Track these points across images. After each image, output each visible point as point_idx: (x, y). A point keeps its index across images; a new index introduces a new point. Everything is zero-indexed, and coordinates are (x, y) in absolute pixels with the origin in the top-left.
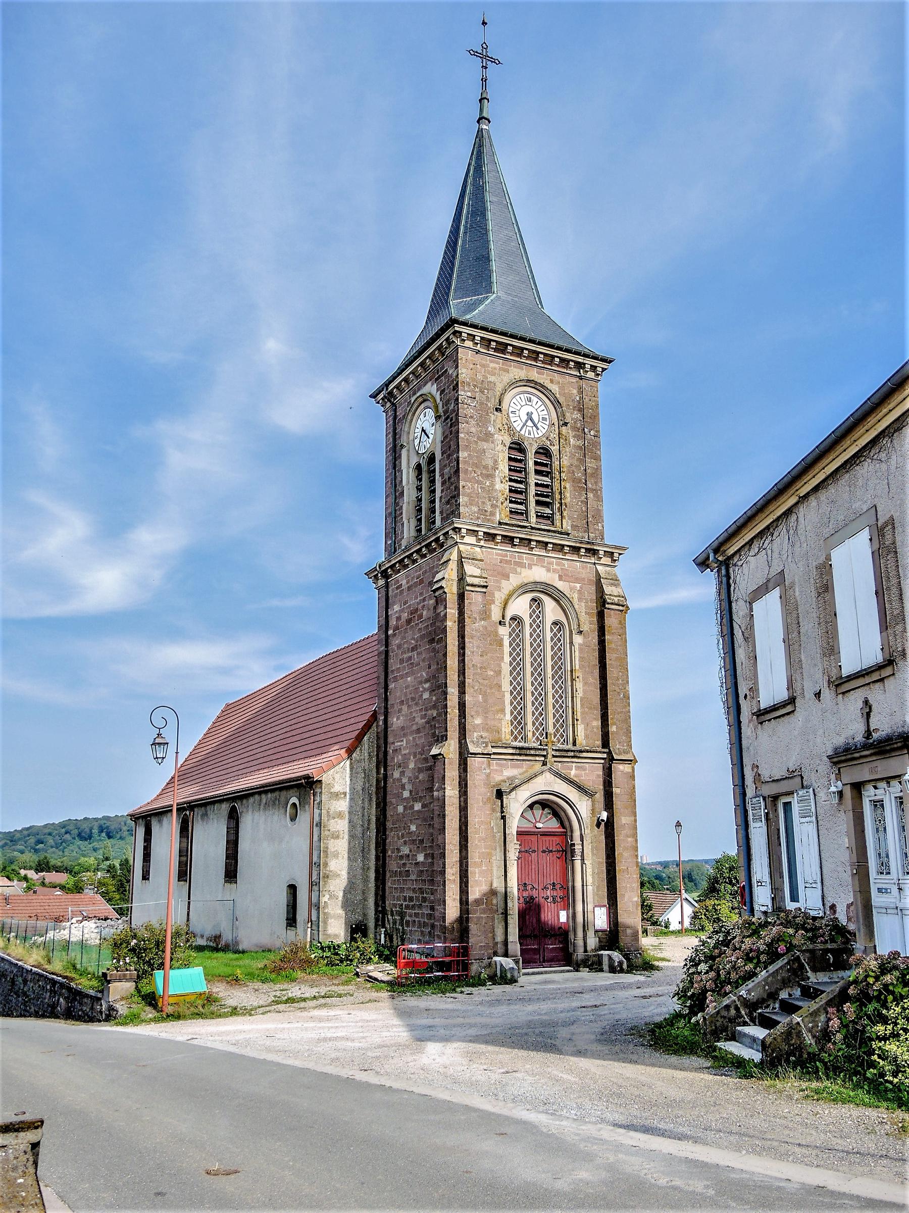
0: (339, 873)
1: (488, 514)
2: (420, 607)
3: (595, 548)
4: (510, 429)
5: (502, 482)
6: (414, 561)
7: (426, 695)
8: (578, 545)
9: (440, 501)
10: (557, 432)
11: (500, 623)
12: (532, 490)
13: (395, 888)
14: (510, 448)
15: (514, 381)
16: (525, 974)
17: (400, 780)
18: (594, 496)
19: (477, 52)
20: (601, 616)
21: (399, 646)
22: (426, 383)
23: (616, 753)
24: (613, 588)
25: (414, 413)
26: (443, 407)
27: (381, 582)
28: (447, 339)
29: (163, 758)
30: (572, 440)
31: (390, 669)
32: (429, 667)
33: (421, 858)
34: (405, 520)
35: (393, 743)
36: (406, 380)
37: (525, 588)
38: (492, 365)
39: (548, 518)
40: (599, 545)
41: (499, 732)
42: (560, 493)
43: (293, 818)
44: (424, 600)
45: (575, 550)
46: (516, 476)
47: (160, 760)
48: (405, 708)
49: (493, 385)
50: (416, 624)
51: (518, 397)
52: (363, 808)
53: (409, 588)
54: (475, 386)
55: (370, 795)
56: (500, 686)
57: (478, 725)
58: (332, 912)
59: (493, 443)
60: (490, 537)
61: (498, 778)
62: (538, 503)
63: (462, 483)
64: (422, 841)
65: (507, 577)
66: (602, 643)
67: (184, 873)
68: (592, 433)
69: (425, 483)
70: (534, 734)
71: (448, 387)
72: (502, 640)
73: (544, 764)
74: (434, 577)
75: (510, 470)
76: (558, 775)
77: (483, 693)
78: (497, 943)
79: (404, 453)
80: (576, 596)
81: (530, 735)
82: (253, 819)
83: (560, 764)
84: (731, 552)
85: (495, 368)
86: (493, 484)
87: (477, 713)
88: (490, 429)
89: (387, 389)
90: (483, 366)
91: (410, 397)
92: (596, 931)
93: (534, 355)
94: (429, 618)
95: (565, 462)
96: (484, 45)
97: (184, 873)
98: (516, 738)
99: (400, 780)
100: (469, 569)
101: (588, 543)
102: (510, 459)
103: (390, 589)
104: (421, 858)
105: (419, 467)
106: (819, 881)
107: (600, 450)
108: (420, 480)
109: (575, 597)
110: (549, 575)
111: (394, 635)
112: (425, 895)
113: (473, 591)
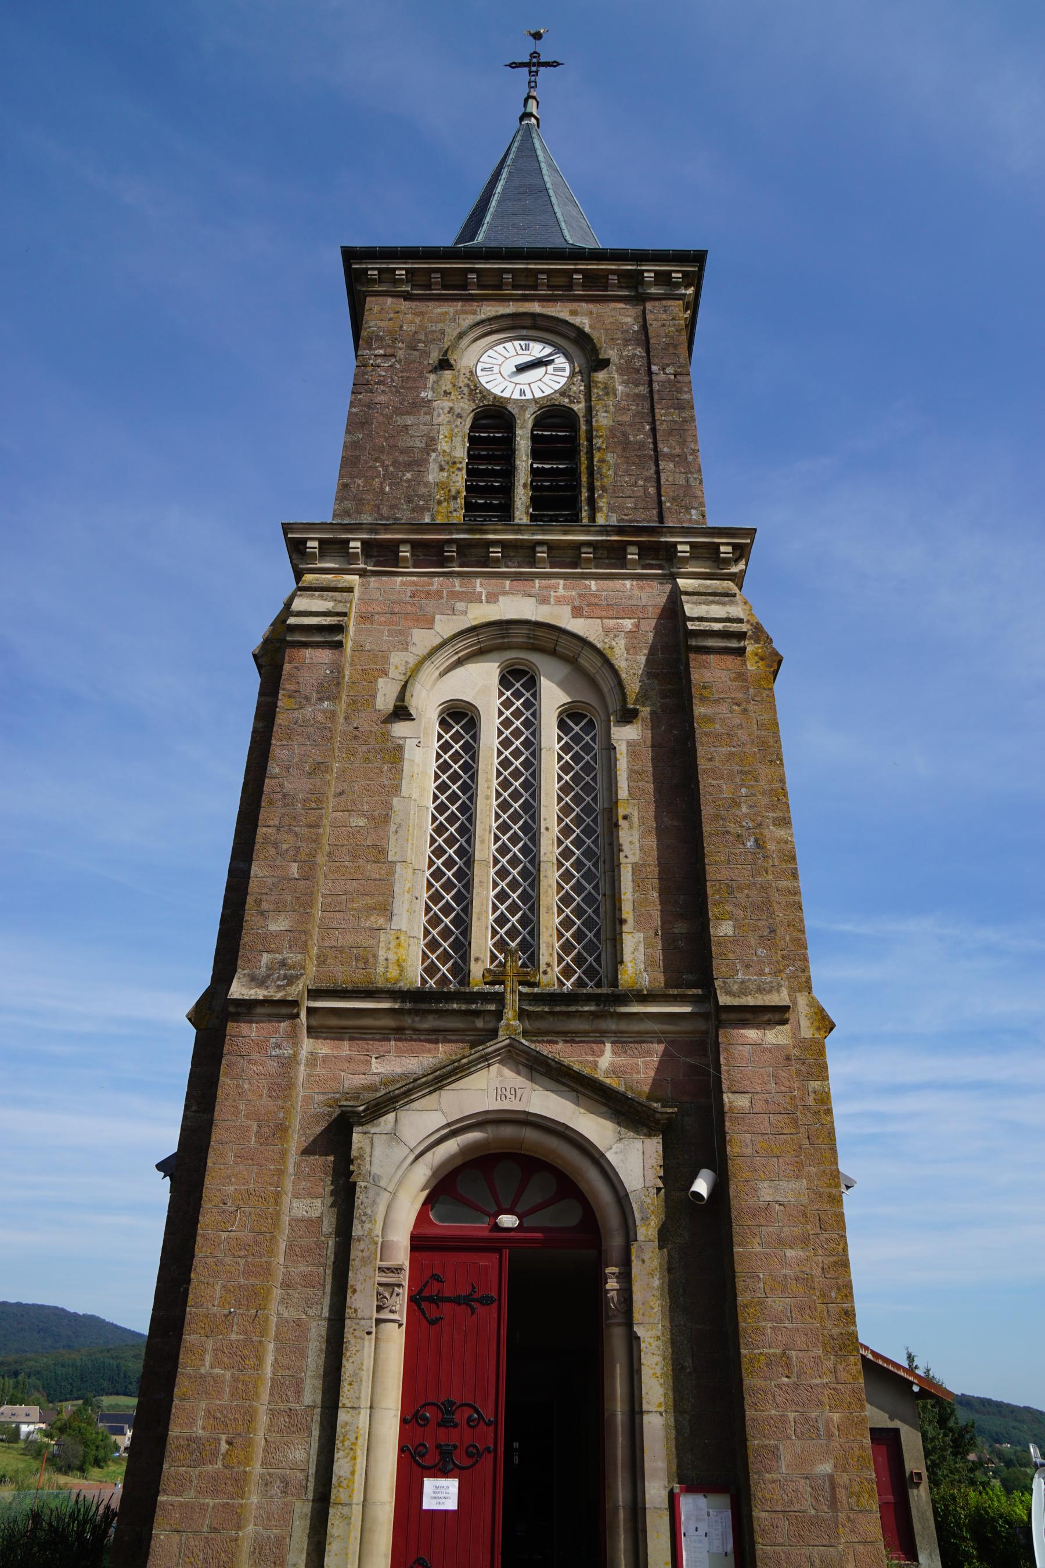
4: (475, 390)
40: (672, 531)
65: (428, 623)
77: (303, 856)
87: (280, 908)
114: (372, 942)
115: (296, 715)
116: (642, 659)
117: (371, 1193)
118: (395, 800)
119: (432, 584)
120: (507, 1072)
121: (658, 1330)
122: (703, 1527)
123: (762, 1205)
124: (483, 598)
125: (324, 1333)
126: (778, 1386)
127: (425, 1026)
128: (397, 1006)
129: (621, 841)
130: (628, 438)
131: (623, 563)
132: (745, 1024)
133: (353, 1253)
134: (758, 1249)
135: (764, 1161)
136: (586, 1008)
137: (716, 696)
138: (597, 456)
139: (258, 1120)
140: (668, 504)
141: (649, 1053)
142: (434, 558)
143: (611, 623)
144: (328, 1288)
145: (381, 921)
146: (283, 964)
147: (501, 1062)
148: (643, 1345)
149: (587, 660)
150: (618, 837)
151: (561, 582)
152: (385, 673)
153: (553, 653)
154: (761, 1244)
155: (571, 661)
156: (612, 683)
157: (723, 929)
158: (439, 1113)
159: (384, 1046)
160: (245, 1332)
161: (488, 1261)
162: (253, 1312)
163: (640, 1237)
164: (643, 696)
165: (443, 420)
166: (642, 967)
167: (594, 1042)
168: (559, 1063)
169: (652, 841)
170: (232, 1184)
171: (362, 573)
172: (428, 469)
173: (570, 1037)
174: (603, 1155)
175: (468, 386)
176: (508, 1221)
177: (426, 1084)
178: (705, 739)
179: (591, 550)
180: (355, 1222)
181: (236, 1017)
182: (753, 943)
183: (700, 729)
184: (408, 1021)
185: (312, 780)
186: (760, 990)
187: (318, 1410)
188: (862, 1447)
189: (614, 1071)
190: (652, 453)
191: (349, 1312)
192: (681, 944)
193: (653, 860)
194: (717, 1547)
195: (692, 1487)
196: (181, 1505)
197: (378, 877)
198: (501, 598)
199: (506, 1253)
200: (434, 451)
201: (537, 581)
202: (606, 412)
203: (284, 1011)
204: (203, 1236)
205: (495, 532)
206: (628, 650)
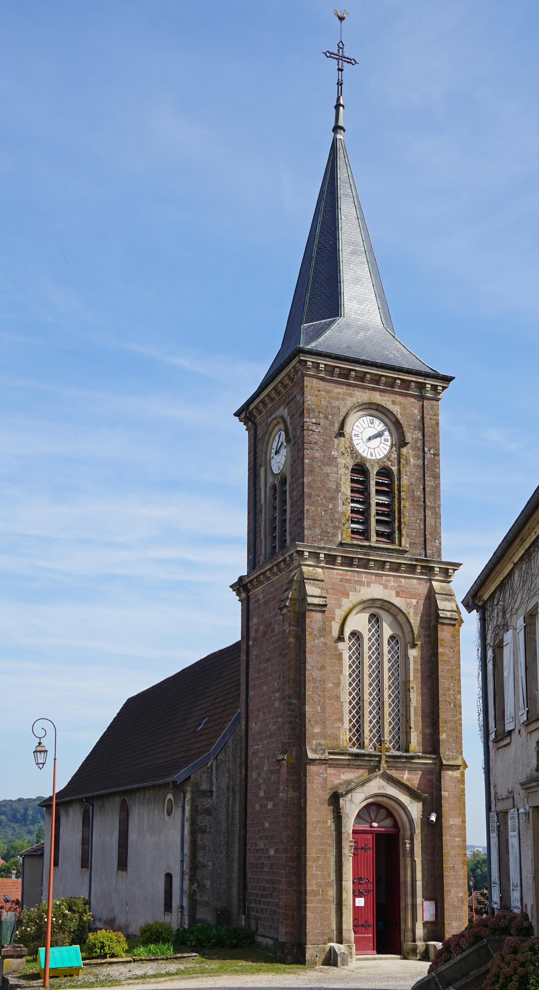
0: (206, 863)
1: (330, 535)
2: (273, 621)
4: (353, 452)
5: (344, 504)
7: (277, 704)
9: (290, 522)
13: (254, 879)
14: (352, 469)
15: (357, 404)
16: (358, 960)
17: (257, 780)
18: (432, 513)
21: (257, 656)
22: (280, 406)
23: (445, 759)
24: (447, 603)
26: (292, 432)
29: (43, 764)
30: (412, 460)
31: (250, 678)
35: (252, 746)
36: (262, 401)
40: (434, 562)
41: (336, 738)
43: (169, 813)
45: (412, 568)
47: (41, 766)
48: (261, 714)
49: (336, 410)
50: (270, 637)
51: (361, 420)
52: (228, 805)
53: (265, 603)
54: (319, 412)
55: (234, 793)
56: (339, 697)
57: (317, 733)
58: (200, 899)
60: (331, 559)
62: (378, 522)
63: (306, 507)
65: (347, 595)
67: (86, 862)
68: (432, 452)
70: (371, 741)
72: (341, 654)
75: (352, 491)
77: (321, 704)
80: (412, 611)
81: (367, 742)
82: (139, 812)
84: (486, 597)
85: (339, 393)
86: (335, 506)
87: (317, 722)
88: (333, 453)
90: (328, 392)
91: (267, 418)
93: (377, 380)
94: (279, 633)
95: (405, 481)
97: (86, 862)
98: (354, 745)
99: (257, 780)
102: (353, 481)
103: (251, 602)
104: (272, 852)
105: (274, 487)
106: (519, 885)
107: (439, 468)
110: (387, 591)
111: (253, 645)
112: (275, 886)
114: (338, 732)
115: (313, 643)
116: (419, 619)
117: (347, 819)
118: (341, 676)
119: (347, 575)
120: (381, 781)
121: (420, 859)
122: (428, 909)
123: (450, 825)
124: (365, 584)
125: (334, 860)
126: (452, 875)
127: (357, 764)
128: (350, 758)
129: (411, 697)
130: (414, 494)
131: (414, 572)
132: (448, 770)
133: (343, 837)
134: (448, 838)
135: (451, 812)
136: (403, 760)
137: (445, 645)
138: (402, 503)
139: (319, 798)
140: (428, 536)
141: (417, 774)
142: (347, 562)
143: (408, 600)
144: (335, 847)
146: (320, 744)
147: (379, 777)
148: (417, 863)
149: (400, 617)
150: (410, 695)
151: (392, 578)
152: (334, 619)
153: (388, 611)
154: (449, 836)
155: (395, 616)
156: (409, 630)
157: (443, 736)
158: (363, 794)
159: (344, 770)
160: (323, 861)
161: (369, 837)
162: (324, 856)
163: (416, 832)
164: (419, 636)
165: (342, 471)
166: (416, 744)
167: (403, 770)
168: (397, 779)
169: (420, 698)
170: (314, 818)
171: (322, 568)
172: (338, 502)
173: (396, 768)
174: (406, 807)
175: (350, 447)
176: (375, 824)
177: (361, 785)
178: (441, 663)
179: (405, 567)
180: (343, 828)
181: (309, 764)
182: (451, 741)
183: (440, 658)
184: (352, 762)
185: (321, 672)
186: (453, 759)
187: (335, 881)
188: (465, 889)
189: (408, 780)
190: (423, 504)
191: (343, 854)
193: (420, 706)
194: (431, 913)
195: (426, 900)
196: (313, 906)
197: (338, 707)
198: (371, 585)
199: (374, 834)
201: (384, 577)
202: (406, 475)
203: (324, 762)
204: (309, 834)
205: (373, 556)
206: (414, 614)
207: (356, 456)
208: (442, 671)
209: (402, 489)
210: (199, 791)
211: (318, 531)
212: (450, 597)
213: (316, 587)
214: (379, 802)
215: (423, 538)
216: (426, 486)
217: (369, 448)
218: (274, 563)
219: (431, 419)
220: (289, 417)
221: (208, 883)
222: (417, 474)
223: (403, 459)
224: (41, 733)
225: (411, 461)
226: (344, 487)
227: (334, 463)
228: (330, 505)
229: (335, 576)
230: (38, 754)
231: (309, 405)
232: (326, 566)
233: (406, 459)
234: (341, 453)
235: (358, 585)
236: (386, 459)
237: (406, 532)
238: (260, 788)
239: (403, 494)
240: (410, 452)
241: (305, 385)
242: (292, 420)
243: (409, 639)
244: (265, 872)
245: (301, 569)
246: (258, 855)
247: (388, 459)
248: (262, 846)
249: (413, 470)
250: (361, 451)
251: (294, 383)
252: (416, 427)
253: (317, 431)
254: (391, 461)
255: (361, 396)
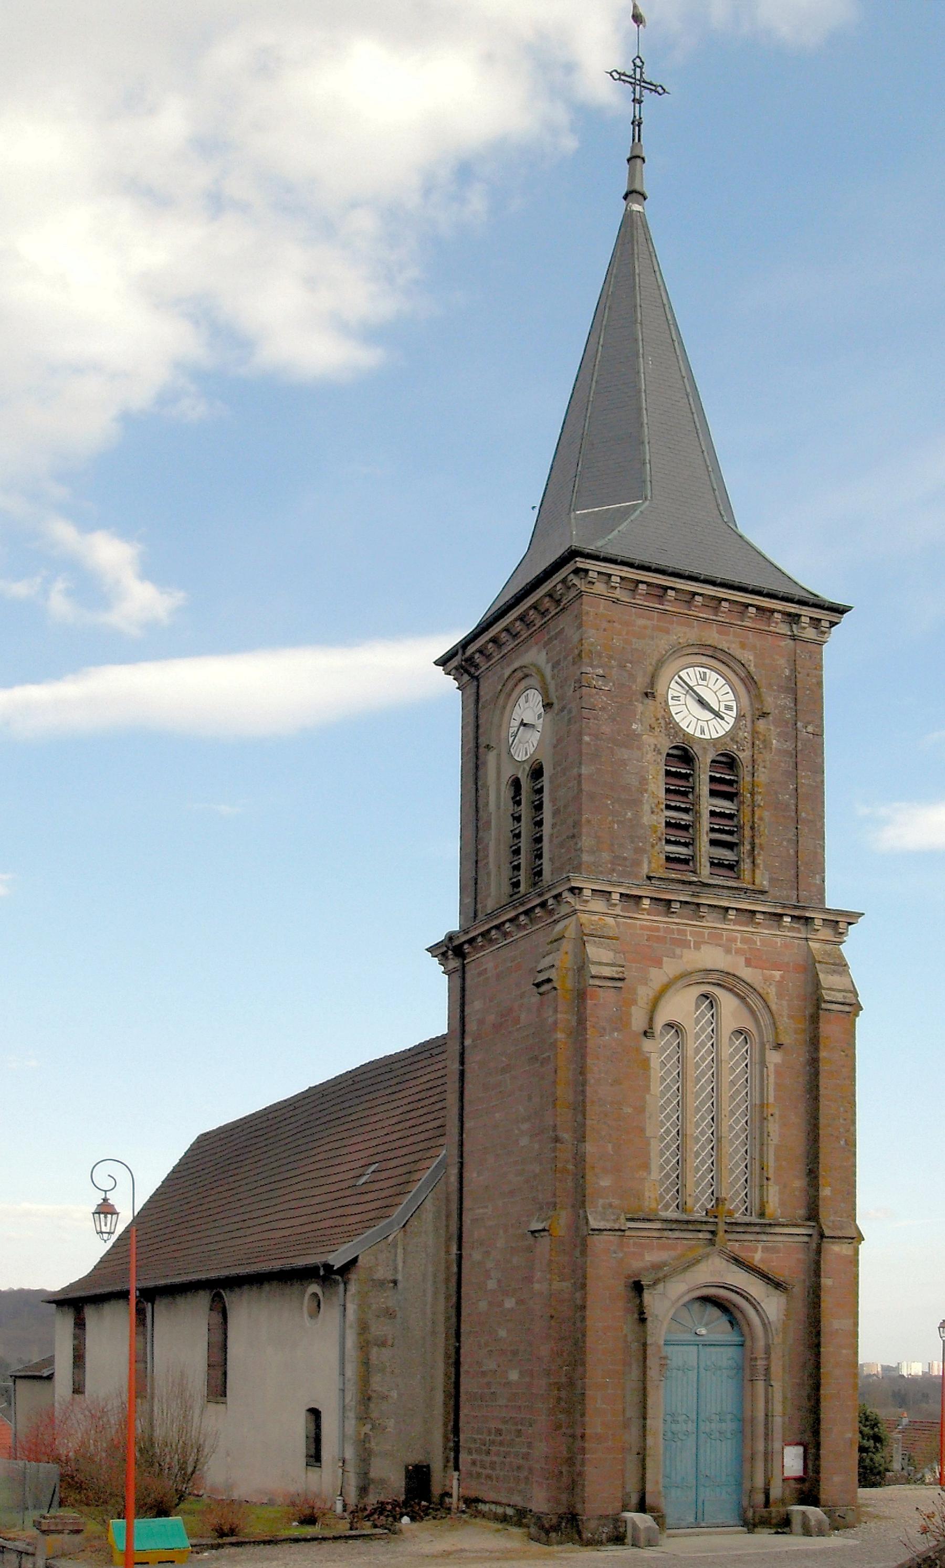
3: (807, 915)
4: (671, 726)
5: (652, 812)
6: (506, 935)
7: (524, 1141)
8: (779, 911)
9: (551, 841)
10: (749, 729)
11: (645, 1033)
12: (705, 823)
14: (668, 755)
19: (624, 74)
20: (815, 1019)
25: (509, 695)
27: (454, 963)
28: (564, 581)
30: (774, 741)
32: (530, 1098)
33: (514, 1376)
34: (492, 866)
36: (494, 640)
37: (684, 978)
38: (641, 622)
39: (731, 867)
40: (814, 909)
42: (752, 828)
44: (522, 996)
46: (677, 802)
53: (498, 976)
59: (639, 748)
61: (636, 1265)
62: (713, 793)
64: (515, 1353)
65: (658, 963)
66: (814, 1062)
69: (525, 810)
71: (565, 658)
73: (712, 1242)
74: (538, 962)
75: (668, 791)
76: (738, 1261)
78: (628, 1494)
79: (491, 758)
83: (737, 1244)
85: (645, 627)
89: (464, 653)
92: (785, 1480)
95: (762, 776)
96: (638, 62)
100: (593, 951)
101: (796, 907)
102: (668, 773)
104: (514, 1376)
108: (518, 803)
109: (772, 993)
113: (600, 987)
118: (647, 1096)
124: (692, 945)
130: (777, 798)
145: (645, 1174)
146: (611, 1205)
166: (777, 1205)
175: (664, 718)
189: (762, 1260)
192: (797, 1193)
200: (646, 791)
202: (764, 767)
207: (676, 732)
208: (826, 1088)
209: (756, 789)
210: (373, 1280)
211: (606, 856)
212: (841, 969)
213: (605, 948)
214: (719, 1298)
215: (793, 872)
216: (799, 786)
217: (698, 719)
218: (521, 909)
219: (808, 675)
220: (550, 664)
221: (391, 1423)
222: (783, 765)
223: (759, 740)
224: (109, 1184)
225: (772, 744)
226: (654, 783)
227: (636, 743)
228: (629, 814)
229: (638, 932)
230: (102, 1216)
231: (592, 644)
232: (621, 914)
233: (764, 741)
234: (648, 727)
235: (679, 946)
236: (728, 739)
237: (764, 861)
238: (488, 1277)
239: (758, 798)
240: (772, 728)
241: (584, 612)
242: (556, 671)
243: (769, 1036)
244: (500, 1406)
245: (578, 919)
246: (486, 1380)
247: (732, 739)
248: (492, 1366)
249: (776, 758)
250: (683, 725)
251: (561, 607)
252: (782, 687)
253: (606, 689)
254: (737, 742)
255: (685, 633)
